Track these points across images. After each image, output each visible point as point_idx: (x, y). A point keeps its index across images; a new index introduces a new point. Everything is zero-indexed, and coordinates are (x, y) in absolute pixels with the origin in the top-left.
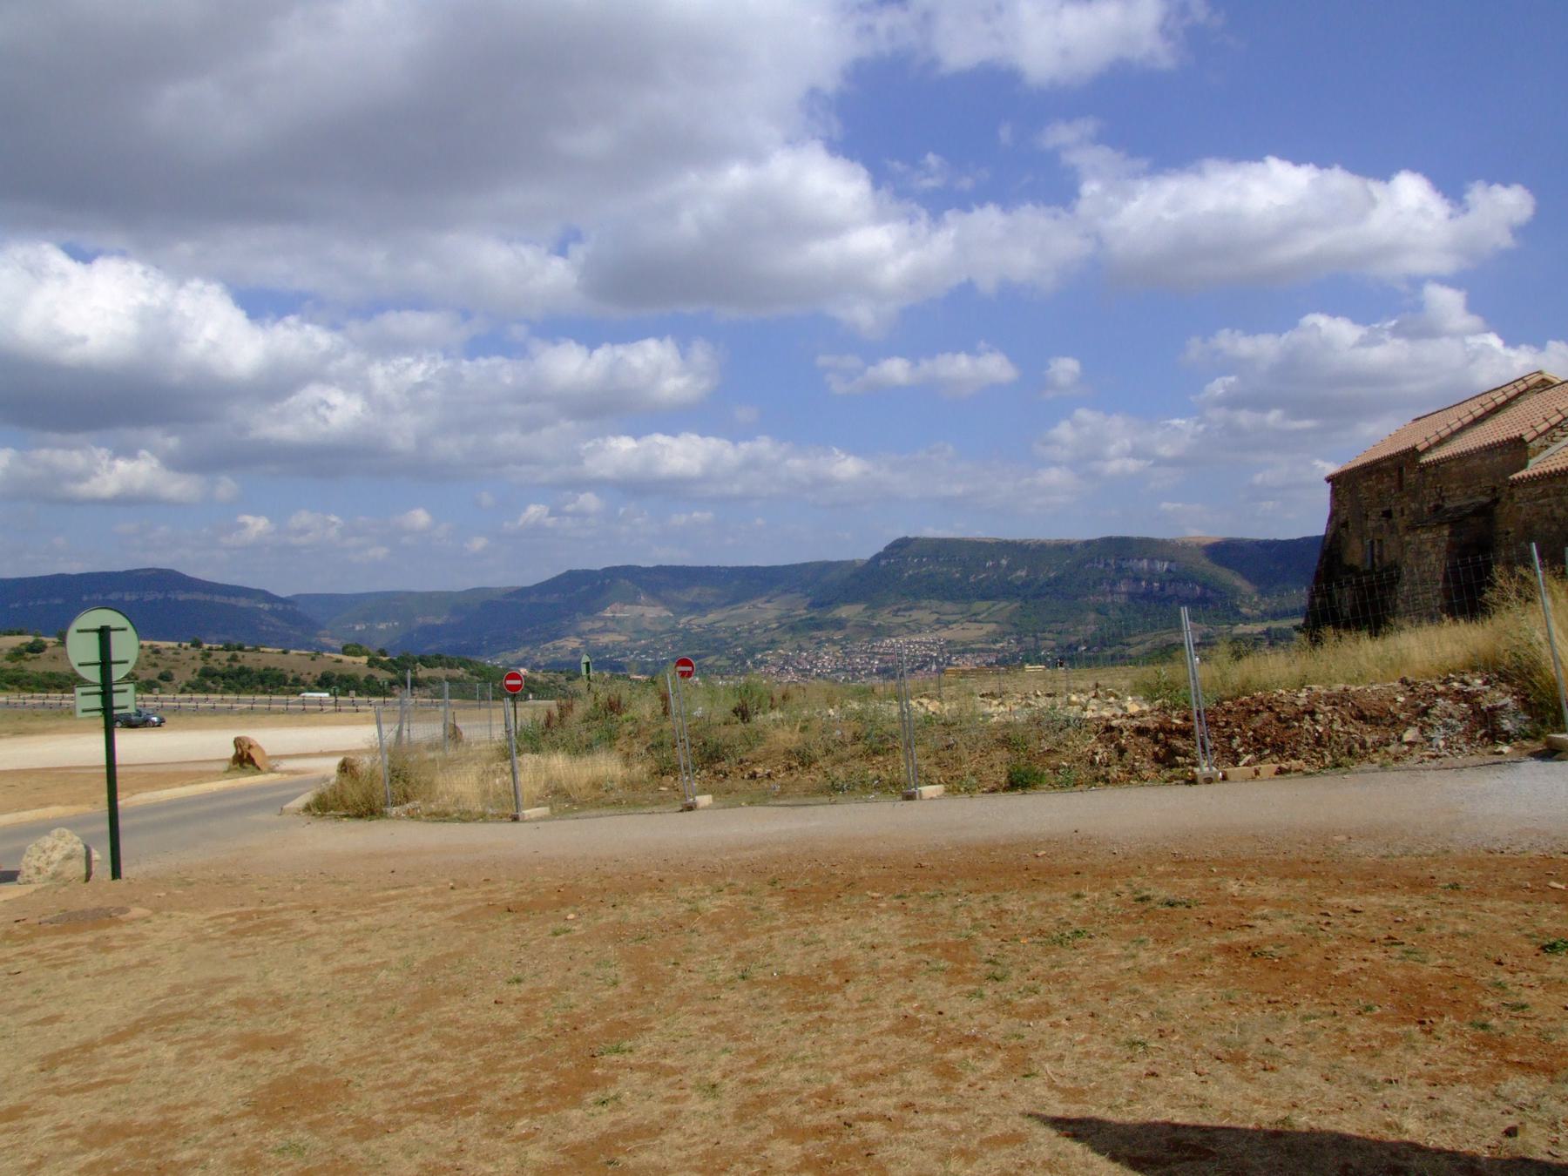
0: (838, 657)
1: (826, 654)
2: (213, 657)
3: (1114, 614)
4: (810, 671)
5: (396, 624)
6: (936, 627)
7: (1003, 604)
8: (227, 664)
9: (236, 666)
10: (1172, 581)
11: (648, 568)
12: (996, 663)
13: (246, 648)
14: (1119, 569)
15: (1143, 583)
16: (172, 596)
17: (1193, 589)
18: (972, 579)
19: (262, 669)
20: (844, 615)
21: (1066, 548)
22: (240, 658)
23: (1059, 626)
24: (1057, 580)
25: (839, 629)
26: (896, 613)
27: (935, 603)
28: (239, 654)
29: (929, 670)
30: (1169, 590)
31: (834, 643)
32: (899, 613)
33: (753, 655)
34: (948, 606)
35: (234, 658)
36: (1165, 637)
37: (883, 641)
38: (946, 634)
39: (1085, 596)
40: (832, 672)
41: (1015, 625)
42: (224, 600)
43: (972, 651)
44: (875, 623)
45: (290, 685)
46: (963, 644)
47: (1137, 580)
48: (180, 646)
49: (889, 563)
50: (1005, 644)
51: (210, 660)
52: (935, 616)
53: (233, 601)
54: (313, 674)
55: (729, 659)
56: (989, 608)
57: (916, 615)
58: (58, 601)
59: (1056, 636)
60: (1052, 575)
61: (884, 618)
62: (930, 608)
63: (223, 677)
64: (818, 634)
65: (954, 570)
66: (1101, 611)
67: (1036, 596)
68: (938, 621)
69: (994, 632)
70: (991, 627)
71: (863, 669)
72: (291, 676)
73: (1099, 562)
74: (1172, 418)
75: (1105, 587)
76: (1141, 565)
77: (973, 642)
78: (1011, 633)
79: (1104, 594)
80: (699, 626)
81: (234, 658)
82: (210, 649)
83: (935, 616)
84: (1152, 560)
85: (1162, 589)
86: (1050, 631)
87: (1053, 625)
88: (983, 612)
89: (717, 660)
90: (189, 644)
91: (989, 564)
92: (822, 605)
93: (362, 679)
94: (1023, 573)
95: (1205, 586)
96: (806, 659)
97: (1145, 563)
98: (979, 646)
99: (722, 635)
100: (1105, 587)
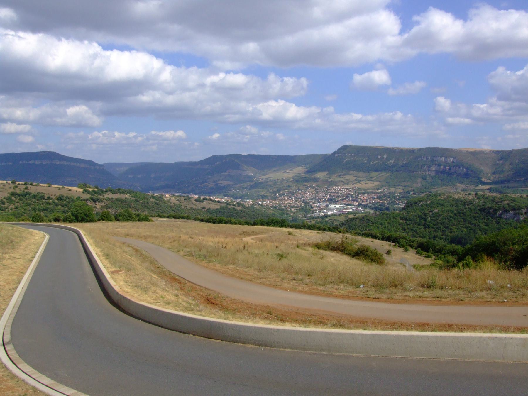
0: (313, 194)
1: (309, 192)
2: (18, 188)
3: (429, 179)
4: (301, 199)
5: (145, 175)
6: (355, 182)
7: (383, 174)
8: (23, 190)
9: (26, 191)
10: (454, 166)
11: (245, 155)
12: (377, 198)
13: (34, 184)
14: (432, 161)
15: (442, 167)
16: (53, 162)
17: (463, 170)
18: (371, 163)
19: (36, 193)
20: (318, 177)
21: (412, 151)
22: (29, 188)
23: (406, 184)
24: (406, 165)
25: (316, 182)
26: (339, 176)
27: (356, 172)
28: (29, 186)
29: (349, 200)
30: (453, 170)
31: (313, 187)
32: (341, 176)
33: (280, 191)
34: (361, 174)
35: (27, 188)
36: (446, 190)
37: (332, 187)
38: (358, 185)
39: (417, 172)
40: (310, 199)
41: (387, 182)
42: (75, 164)
43: (368, 193)
44: (330, 180)
45: (46, 200)
46: (364, 190)
47: (439, 165)
48: (7, 183)
49: (339, 156)
50: (382, 190)
51: (17, 189)
52: (355, 178)
53: (78, 165)
54: (56, 195)
55: (270, 193)
56: (377, 175)
57: (347, 177)
58: (11, 163)
59: (403, 188)
60: (404, 162)
61: (334, 178)
62: (353, 175)
63: (19, 196)
64: (307, 184)
65: (365, 159)
66: (424, 178)
67: (397, 171)
68: (356, 180)
69: (378, 185)
70: (377, 183)
71: (322, 199)
72: (46, 196)
73: (424, 157)
74: (477, 103)
75: (426, 168)
76: (441, 159)
77: (369, 189)
78: (385, 186)
79: (425, 171)
80: (262, 179)
81: (27, 188)
82: (19, 184)
83: (355, 178)
84: (446, 157)
85: (450, 169)
86: (402, 186)
87: (403, 183)
88: (375, 177)
89: (265, 193)
90: (10, 182)
91: (379, 157)
92: (311, 172)
93: (75, 198)
94: (393, 161)
95: (467, 169)
96: (300, 194)
97: (443, 159)
98: (371, 191)
99: (270, 183)
100: (426, 168)
